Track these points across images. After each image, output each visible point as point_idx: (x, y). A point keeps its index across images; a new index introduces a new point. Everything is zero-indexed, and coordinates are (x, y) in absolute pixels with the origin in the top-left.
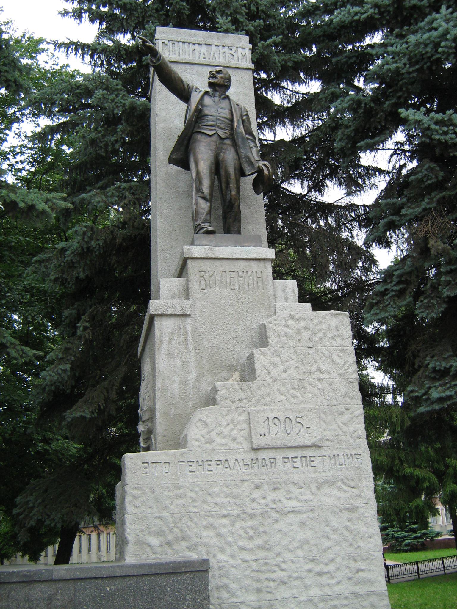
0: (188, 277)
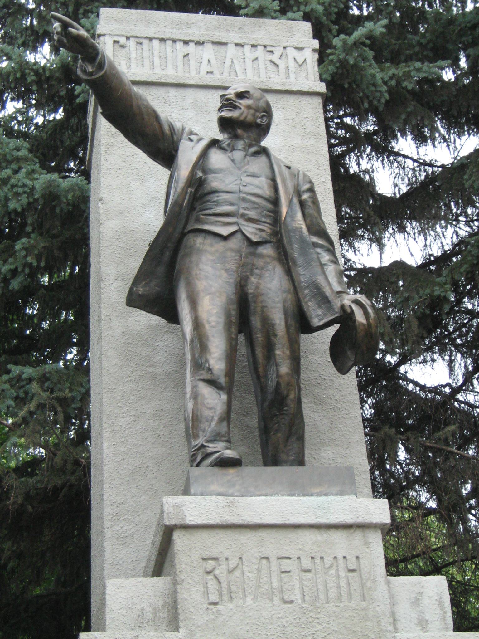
0: (175, 575)
